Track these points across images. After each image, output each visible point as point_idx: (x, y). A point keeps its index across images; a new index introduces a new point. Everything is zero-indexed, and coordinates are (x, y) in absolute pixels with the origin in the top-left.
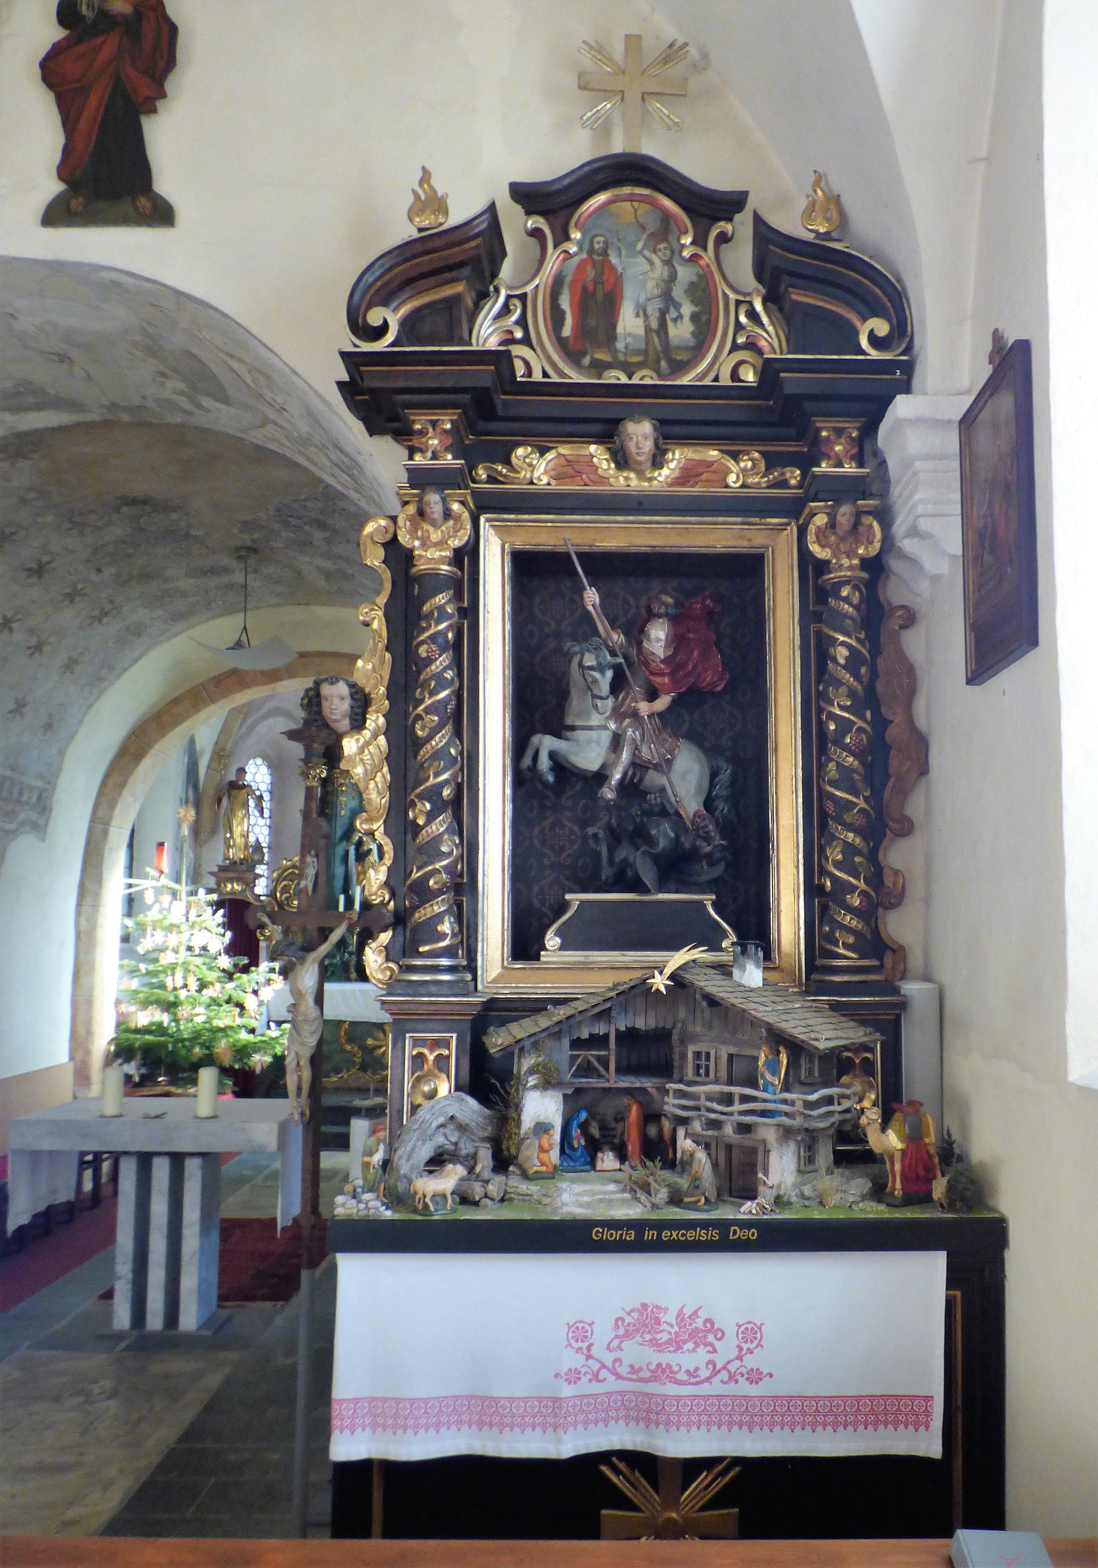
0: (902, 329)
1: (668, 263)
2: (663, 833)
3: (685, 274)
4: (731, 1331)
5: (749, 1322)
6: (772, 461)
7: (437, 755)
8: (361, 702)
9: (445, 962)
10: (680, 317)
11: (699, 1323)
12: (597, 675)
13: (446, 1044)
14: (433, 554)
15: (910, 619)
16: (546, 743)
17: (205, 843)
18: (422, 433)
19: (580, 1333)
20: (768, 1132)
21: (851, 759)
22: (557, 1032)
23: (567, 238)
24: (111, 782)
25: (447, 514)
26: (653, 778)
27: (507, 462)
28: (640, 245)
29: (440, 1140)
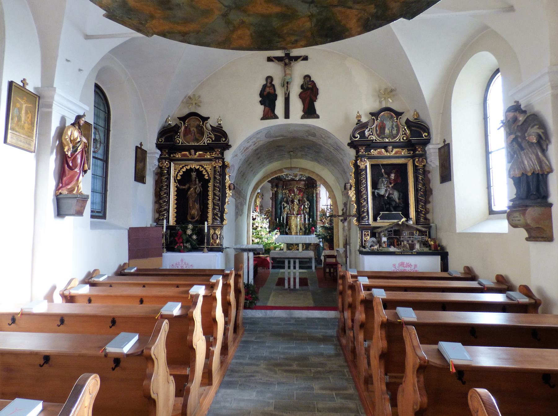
0: (429, 134)
1: (392, 122)
2: (394, 204)
3: (395, 124)
4: (413, 265)
6: (408, 150)
7: (364, 194)
8: (351, 186)
9: (367, 221)
10: (394, 130)
11: (409, 264)
12: (385, 182)
13: (368, 232)
14: (363, 166)
15: (429, 172)
16: (376, 191)
18: (361, 150)
19: (394, 265)
20: (416, 242)
21: (422, 193)
22: (386, 230)
23: (378, 119)
24: (252, 194)
25: (365, 161)
26: (391, 196)
27: (370, 152)
28: (388, 120)
29: (371, 244)
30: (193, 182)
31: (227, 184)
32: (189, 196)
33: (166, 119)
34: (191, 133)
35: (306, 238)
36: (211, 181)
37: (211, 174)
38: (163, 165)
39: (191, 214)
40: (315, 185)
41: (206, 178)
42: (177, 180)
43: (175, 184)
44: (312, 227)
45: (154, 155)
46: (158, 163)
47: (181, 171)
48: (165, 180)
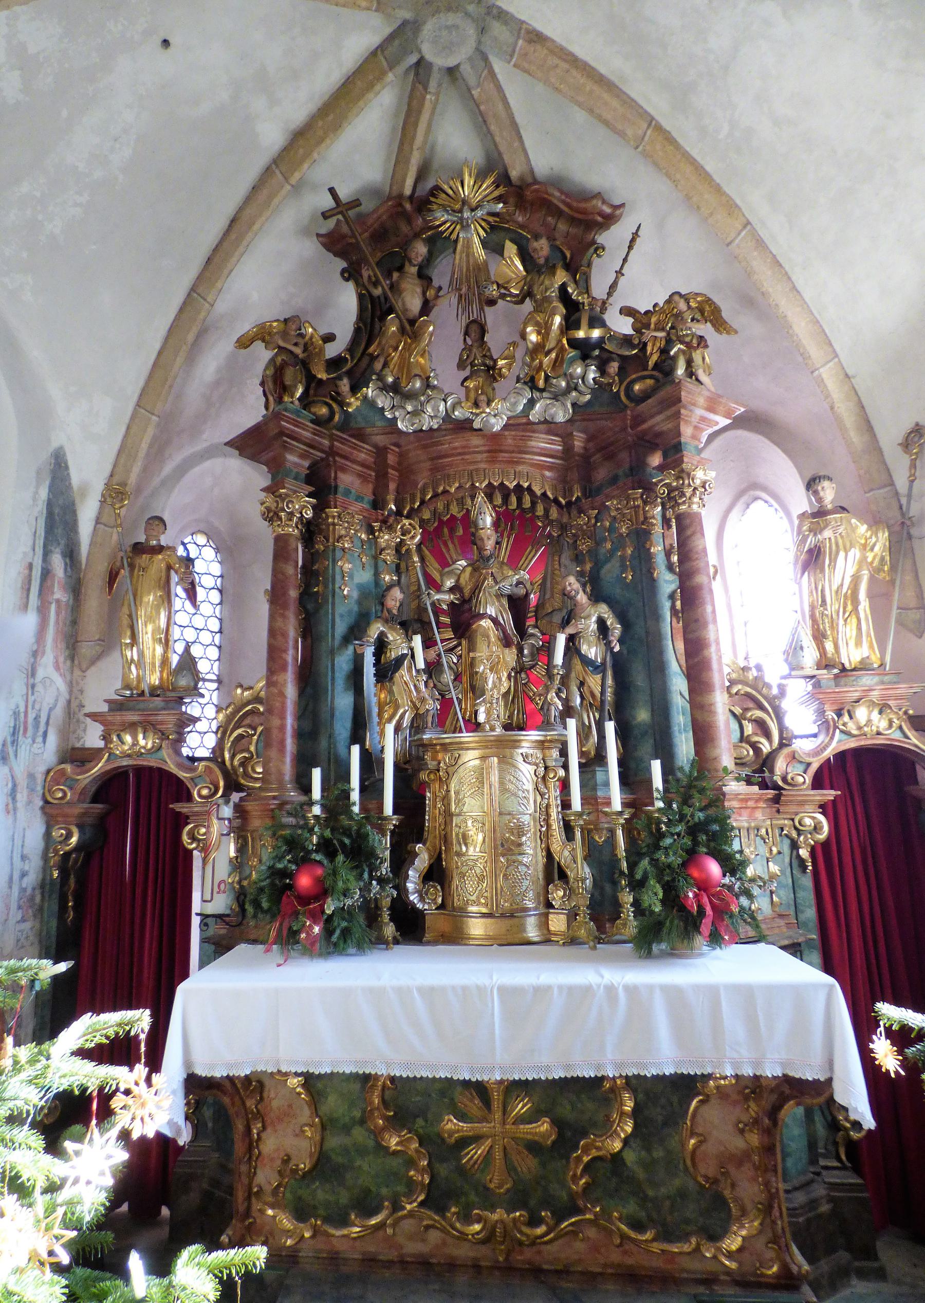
17: (94, 661)
44: (691, 855)
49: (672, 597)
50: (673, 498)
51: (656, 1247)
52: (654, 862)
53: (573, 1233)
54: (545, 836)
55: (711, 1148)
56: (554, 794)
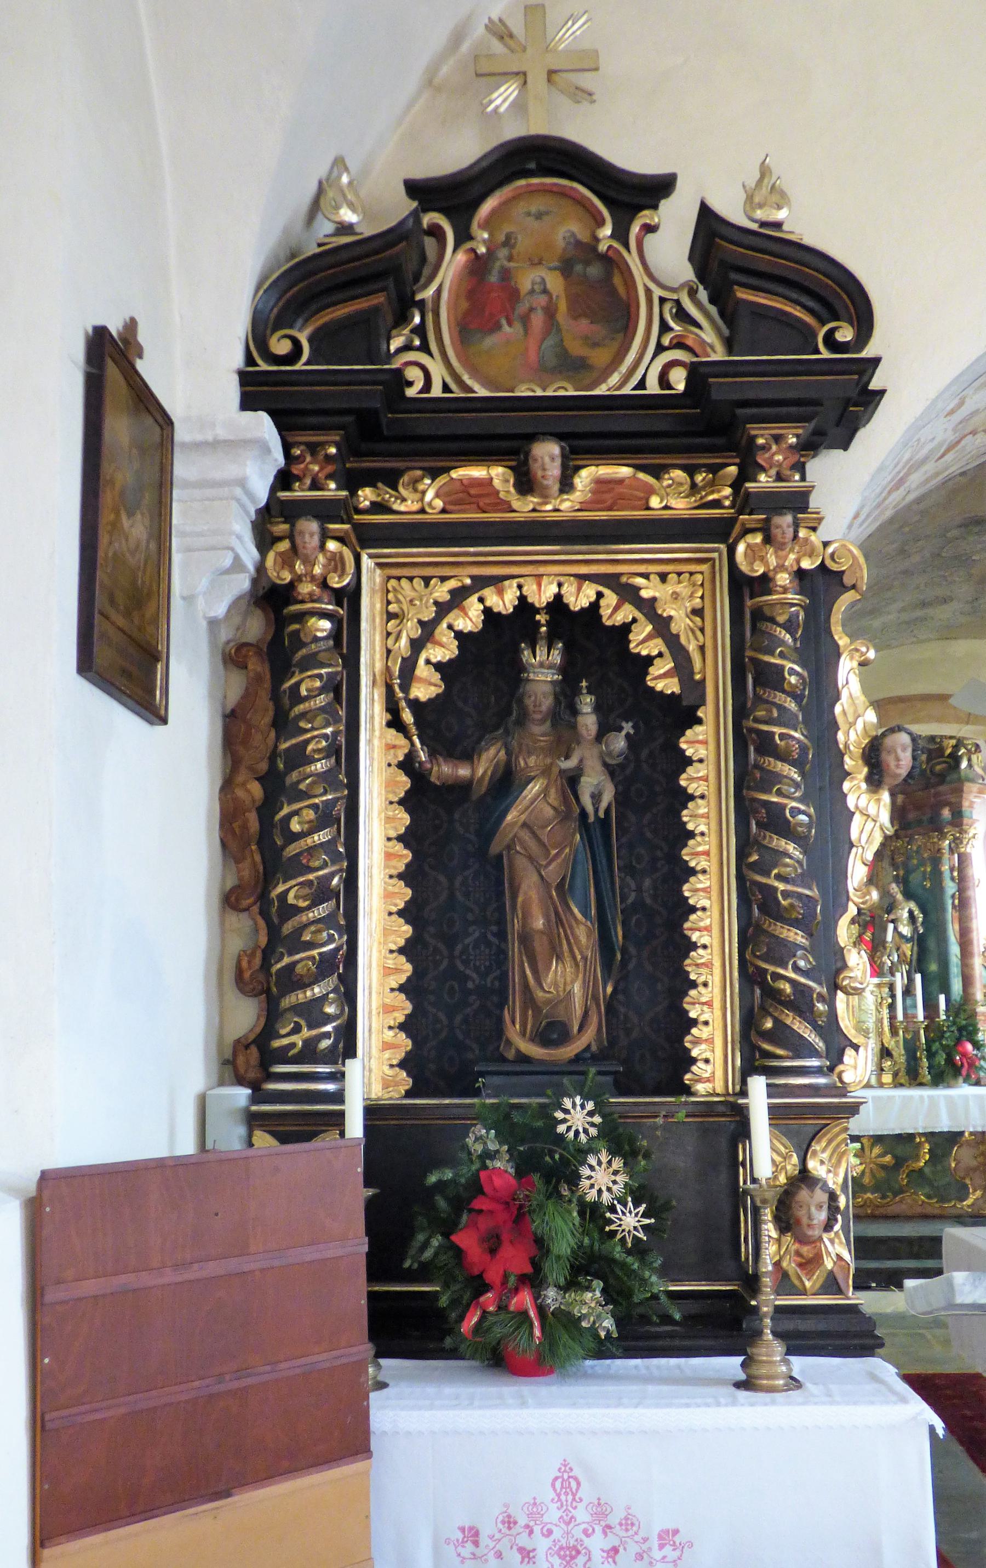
5: (553, 1485)
30: (537, 729)
31: (853, 736)
32: (509, 847)
33: (312, 188)
34: (522, 308)
35: (907, 1100)
36: (700, 714)
37: (702, 648)
38: (299, 567)
39: (540, 994)
40: (946, 813)
41: (660, 686)
42: (415, 705)
43: (400, 740)
44: (958, 1041)
45: (230, 470)
46: (255, 553)
47: (443, 633)
48: (321, 700)
49: (953, 896)
50: (957, 841)
51: (937, 1205)
52: (941, 1044)
53: (901, 1201)
54: (880, 1034)
55: (962, 1165)
56: (885, 1012)
